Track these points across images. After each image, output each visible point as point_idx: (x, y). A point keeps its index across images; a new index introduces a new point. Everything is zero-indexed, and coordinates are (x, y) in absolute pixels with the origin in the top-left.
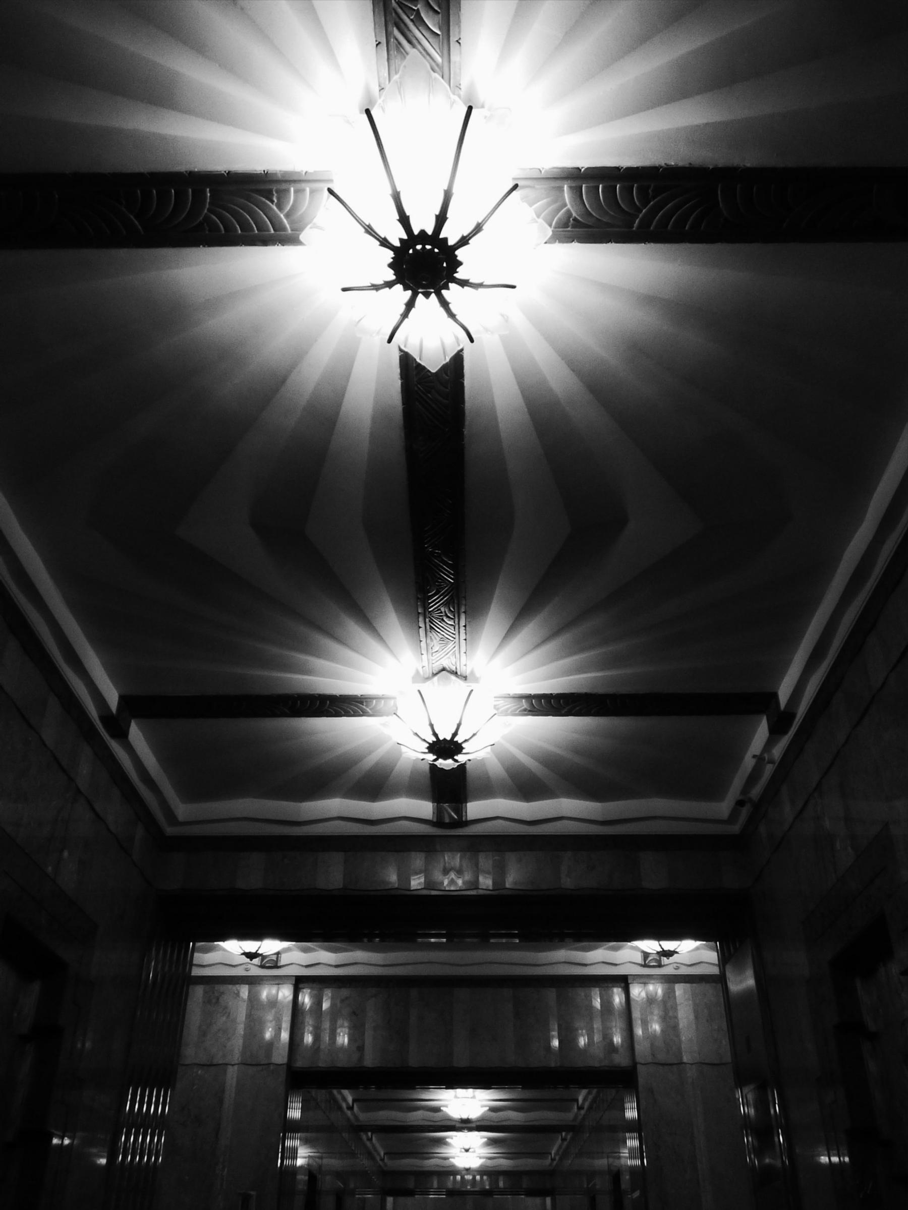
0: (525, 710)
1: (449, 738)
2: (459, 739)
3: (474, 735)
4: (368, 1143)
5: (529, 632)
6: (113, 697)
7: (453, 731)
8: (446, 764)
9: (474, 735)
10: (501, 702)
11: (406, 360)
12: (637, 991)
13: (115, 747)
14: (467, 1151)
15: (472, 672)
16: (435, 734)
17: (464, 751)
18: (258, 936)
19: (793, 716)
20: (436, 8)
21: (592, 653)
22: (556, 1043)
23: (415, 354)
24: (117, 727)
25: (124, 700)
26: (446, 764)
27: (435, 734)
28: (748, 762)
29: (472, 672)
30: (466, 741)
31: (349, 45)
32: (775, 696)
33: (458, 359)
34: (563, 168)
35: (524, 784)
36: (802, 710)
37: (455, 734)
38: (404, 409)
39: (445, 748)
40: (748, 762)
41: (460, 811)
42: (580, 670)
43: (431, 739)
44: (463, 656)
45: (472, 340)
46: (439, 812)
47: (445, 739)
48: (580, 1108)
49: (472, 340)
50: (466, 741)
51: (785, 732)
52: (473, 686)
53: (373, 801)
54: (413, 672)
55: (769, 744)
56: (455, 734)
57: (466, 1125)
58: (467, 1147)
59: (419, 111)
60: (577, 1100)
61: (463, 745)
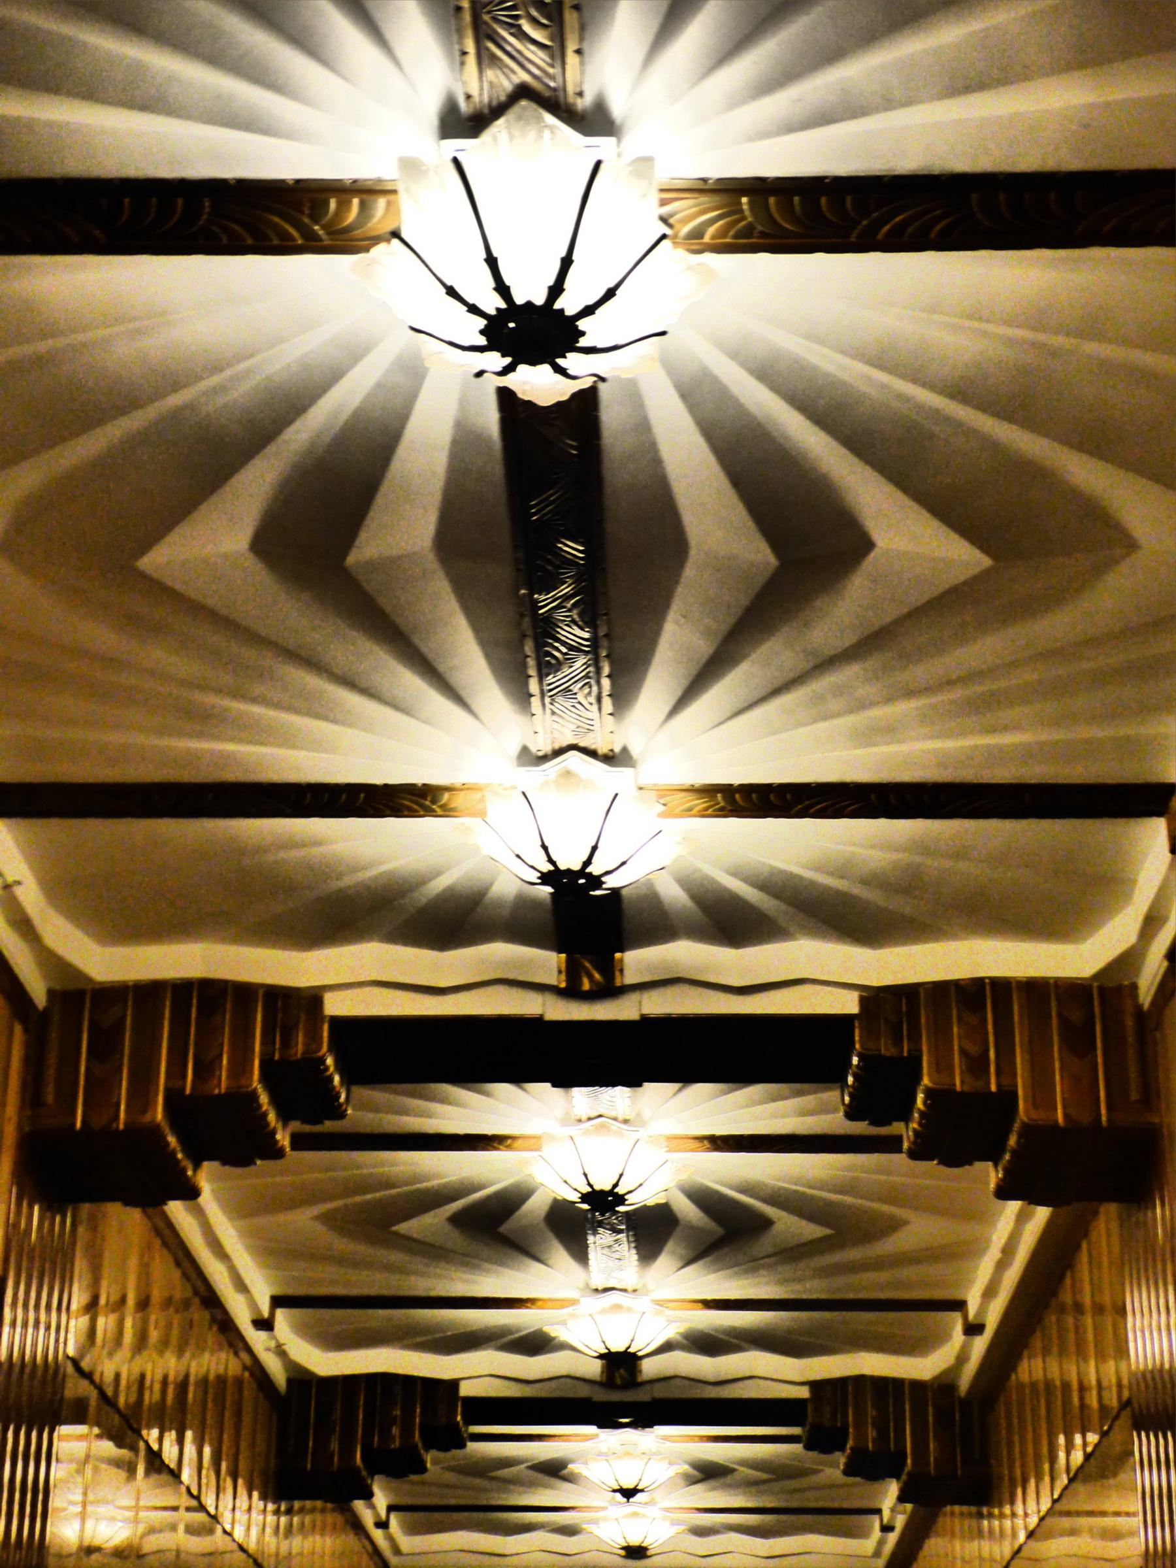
0: (722, 809)
2: (569, 304)
4: (378, 1535)
6: (263, 1297)
7: (614, 1182)
8: (539, 384)
10: (683, 207)
12: (1013, 1231)
14: (629, 1493)
15: (625, 750)
16: (502, 289)
17: (583, 342)
20: (545, 21)
26: (539, 384)
27: (502, 289)
29: (625, 750)
30: (589, 311)
31: (426, 66)
34: (713, 879)
37: (556, 290)
39: (532, 330)
41: (609, 968)
43: (492, 303)
44: (572, 59)
46: (573, 971)
47: (529, 304)
48: (887, 1529)
50: (589, 311)
52: (603, 146)
54: (515, 750)
57: (622, 1394)
58: (628, 1484)
59: (529, 160)
60: (878, 1511)
61: (582, 324)
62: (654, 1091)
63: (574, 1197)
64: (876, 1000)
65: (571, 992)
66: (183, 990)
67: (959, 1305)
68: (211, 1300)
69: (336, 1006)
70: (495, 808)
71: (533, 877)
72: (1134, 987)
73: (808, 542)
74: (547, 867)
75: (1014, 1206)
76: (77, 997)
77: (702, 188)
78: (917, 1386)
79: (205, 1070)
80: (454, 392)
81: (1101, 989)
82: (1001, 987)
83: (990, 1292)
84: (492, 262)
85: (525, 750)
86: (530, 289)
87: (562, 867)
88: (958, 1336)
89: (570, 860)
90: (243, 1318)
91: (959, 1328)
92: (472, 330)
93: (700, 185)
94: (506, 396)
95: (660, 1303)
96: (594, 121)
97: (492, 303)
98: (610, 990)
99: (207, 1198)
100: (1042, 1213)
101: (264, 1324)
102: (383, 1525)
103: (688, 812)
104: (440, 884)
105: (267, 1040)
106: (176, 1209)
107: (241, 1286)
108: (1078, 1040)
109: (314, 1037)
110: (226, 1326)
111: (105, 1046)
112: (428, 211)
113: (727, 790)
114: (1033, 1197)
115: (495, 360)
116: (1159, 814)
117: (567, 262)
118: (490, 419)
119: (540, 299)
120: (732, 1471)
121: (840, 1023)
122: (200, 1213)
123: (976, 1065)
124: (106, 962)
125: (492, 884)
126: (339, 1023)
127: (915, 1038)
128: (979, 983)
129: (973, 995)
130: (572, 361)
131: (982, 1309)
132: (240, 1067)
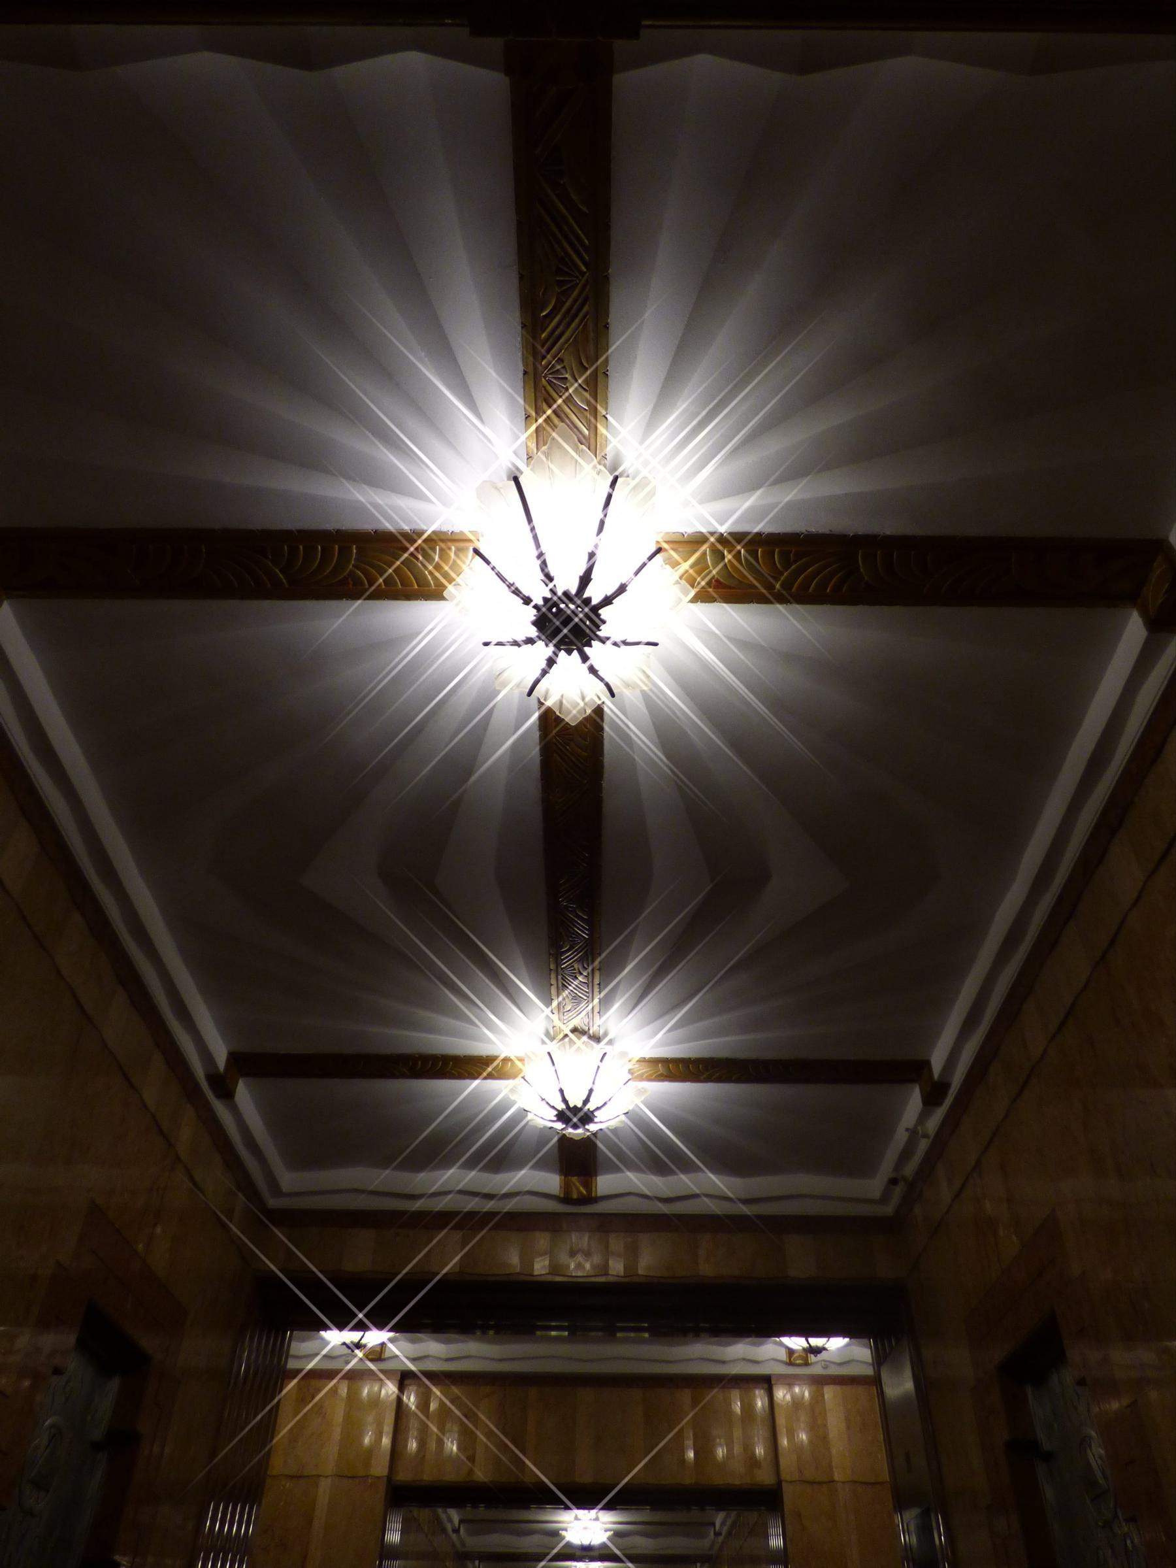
0: (661, 1075)
13: (219, 1107)
27: (565, 1101)
30: (598, 1109)
32: (926, 1064)
33: (599, 711)
37: (586, 1101)
40: (901, 1136)
46: (567, 1187)
48: (717, 1534)
50: (598, 1109)
51: (938, 1103)
55: (923, 1117)
60: (714, 1525)
70: (527, 1070)
74: (561, 1106)
77: (642, 1061)
86: (576, 1100)
90: (449, 1527)
91: (712, 1533)
92: (523, 621)
93: (680, 538)
97: (561, 1106)
102: (456, 1531)
110: (444, 1530)
116: (913, 1081)
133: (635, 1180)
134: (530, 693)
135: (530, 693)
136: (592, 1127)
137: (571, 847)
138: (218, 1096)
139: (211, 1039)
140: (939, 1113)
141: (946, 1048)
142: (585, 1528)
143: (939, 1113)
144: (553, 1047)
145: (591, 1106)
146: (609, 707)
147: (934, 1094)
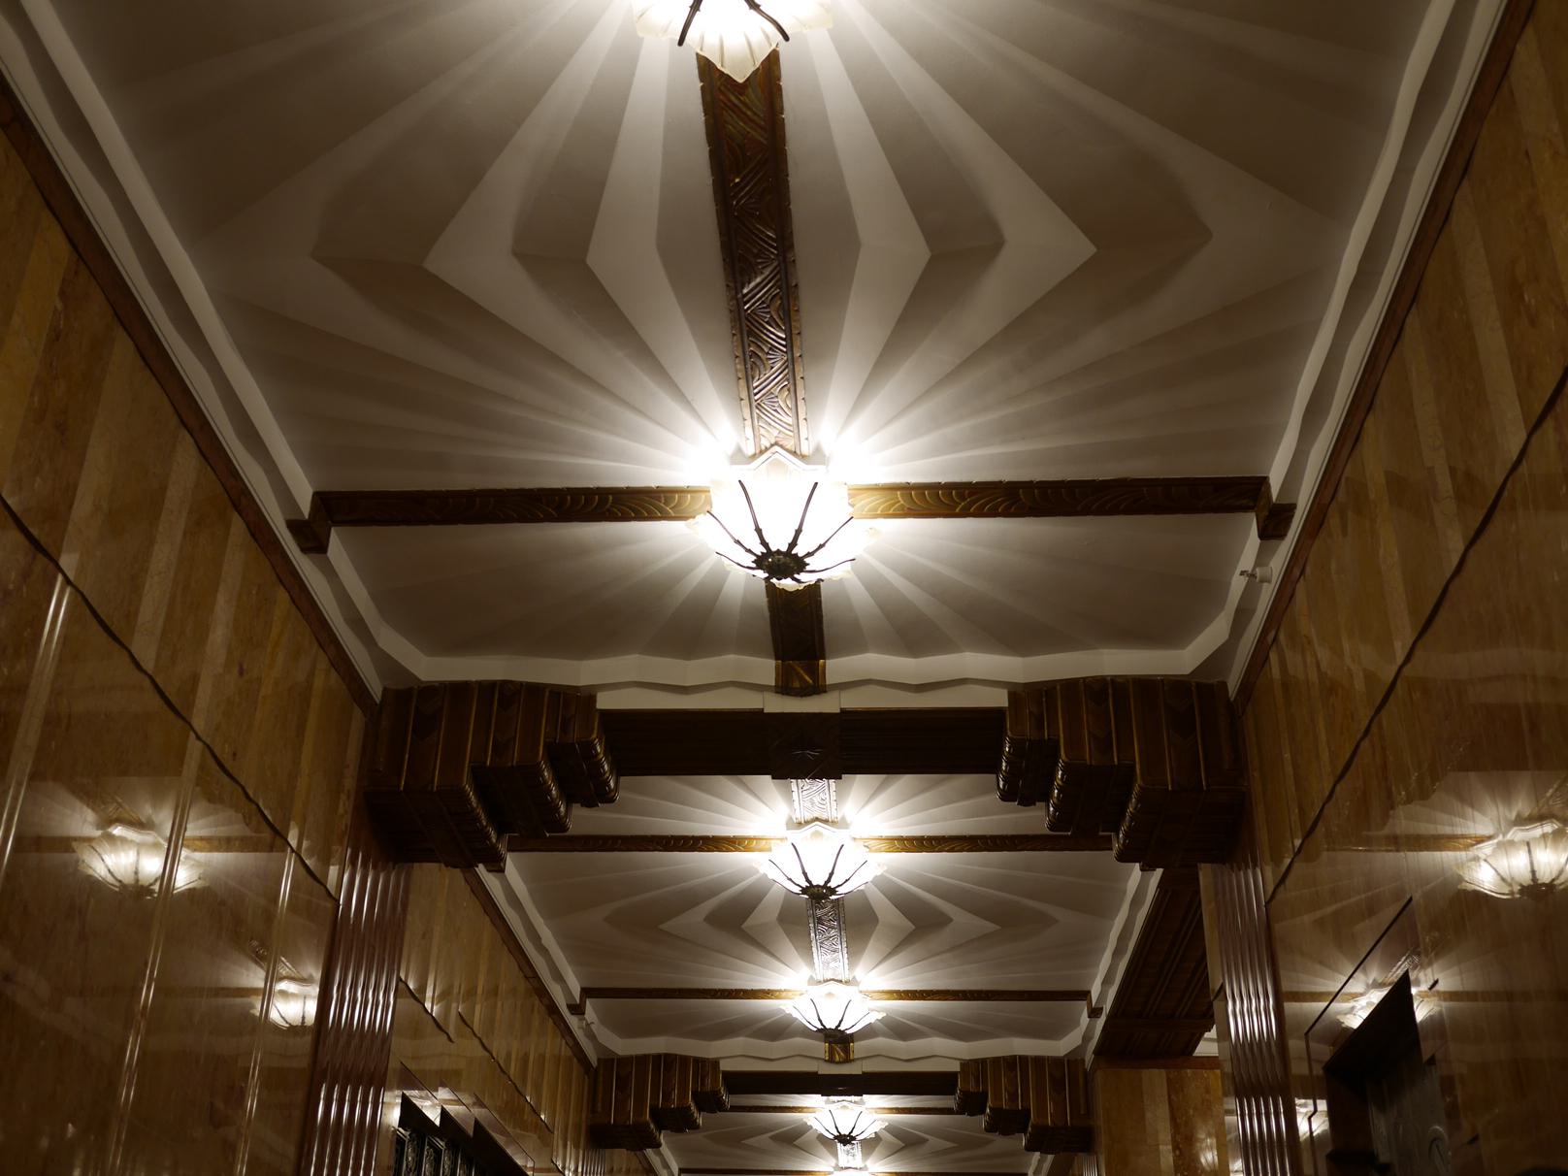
1: (784, 549)
2: (800, 550)
3: (821, 546)
4: (573, 1021)
5: (900, 382)
6: (304, 495)
9: (821, 546)
11: (706, 67)
13: (304, 564)
15: (818, 450)
16: (764, 543)
18: (1109, 1018)
19: (1292, 507)
21: (965, 424)
22: (126, 858)
23: (715, 60)
24: (311, 536)
25: (321, 499)
27: (764, 543)
28: (1238, 584)
30: (809, 554)
32: (1263, 481)
33: (773, 59)
35: (909, 629)
36: (1303, 501)
37: (793, 544)
38: (707, 122)
39: (780, 563)
40: (1238, 584)
41: (817, 673)
42: (954, 446)
43: (759, 550)
45: (786, 38)
46: (831, 1052)
48: (1094, 1013)
49: (786, 38)
50: (809, 554)
51: (1282, 536)
53: (688, 658)
54: (731, 449)
55: (1262, 558)
56: (793, 544)
62: (859, 784)
63: (797, 890)
64: (1023, 695)
65: (784, 688)
66: (488, 688)
67: (1085, 995)
68: (542, 992)
69: (605, 702)
71: (797, 890)
72: (1224, 685)
73: (955, 240)
74: (805, 884)
75: (1037, 1155)
76: (610, 1061)
78: (1057, 1062)
79: (667, 1097)
80: (743, 579)
81: (1198, 685)
82: (1024, 1060)
83: (1107, 981)
84: (759, 531)
85: (739, 450)
86: (779, 543)
87: (774, 549)
88: (1085, 1019)
89: (818, 880)
91: (1085, 1013)
94: (771, 589)
95: (866, 993)
96: (816, 457)
98: (818, 688)
99: (664, 1149)
100: (1050, 1157)
101: (577, 1009)
102: (577, 1009)
103: (879, 851)
104: (677, 556)
105: (695, 1082)
106: (649, 1152)
107: (559, 978)
108: (1058, 1085)
109: (715, 1080)
111: (623, 1086)
112: (726, 503)
113: (901, 839)
114: (1045, 1151)
115: (761, 574)
116: (1246, 509)
117: (798, 532)
118: (763, 599)
119: (784, 549)
120: (925, 1141)
121: (992, 716)
122: (660, 1154)
123: (1013, 1097)
124: (430, 668)
125: (755, 795)
126: (726, 1074)
127: (985, 1083)
128: (1014, 1057)
129: (1013, 1063)
130: (803, 577)
131: (1103, 995)
132: (683, 1095)
133: (873, 662)
134: (681, 42)
135: (681, 42)
136: (806, 578)
137: (798, 691)
138: (304, 550)
139: (287, 475)
140: (1285, 548)
141: (1290, 459)
142: (830, 994)
143: (1285, 548)
144: (746, 472)
145: (832, 884)
146: (785, 50)
147: (1274, 523)
